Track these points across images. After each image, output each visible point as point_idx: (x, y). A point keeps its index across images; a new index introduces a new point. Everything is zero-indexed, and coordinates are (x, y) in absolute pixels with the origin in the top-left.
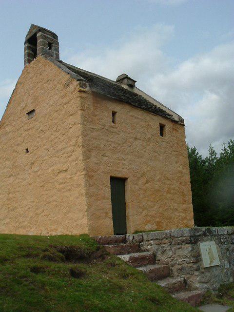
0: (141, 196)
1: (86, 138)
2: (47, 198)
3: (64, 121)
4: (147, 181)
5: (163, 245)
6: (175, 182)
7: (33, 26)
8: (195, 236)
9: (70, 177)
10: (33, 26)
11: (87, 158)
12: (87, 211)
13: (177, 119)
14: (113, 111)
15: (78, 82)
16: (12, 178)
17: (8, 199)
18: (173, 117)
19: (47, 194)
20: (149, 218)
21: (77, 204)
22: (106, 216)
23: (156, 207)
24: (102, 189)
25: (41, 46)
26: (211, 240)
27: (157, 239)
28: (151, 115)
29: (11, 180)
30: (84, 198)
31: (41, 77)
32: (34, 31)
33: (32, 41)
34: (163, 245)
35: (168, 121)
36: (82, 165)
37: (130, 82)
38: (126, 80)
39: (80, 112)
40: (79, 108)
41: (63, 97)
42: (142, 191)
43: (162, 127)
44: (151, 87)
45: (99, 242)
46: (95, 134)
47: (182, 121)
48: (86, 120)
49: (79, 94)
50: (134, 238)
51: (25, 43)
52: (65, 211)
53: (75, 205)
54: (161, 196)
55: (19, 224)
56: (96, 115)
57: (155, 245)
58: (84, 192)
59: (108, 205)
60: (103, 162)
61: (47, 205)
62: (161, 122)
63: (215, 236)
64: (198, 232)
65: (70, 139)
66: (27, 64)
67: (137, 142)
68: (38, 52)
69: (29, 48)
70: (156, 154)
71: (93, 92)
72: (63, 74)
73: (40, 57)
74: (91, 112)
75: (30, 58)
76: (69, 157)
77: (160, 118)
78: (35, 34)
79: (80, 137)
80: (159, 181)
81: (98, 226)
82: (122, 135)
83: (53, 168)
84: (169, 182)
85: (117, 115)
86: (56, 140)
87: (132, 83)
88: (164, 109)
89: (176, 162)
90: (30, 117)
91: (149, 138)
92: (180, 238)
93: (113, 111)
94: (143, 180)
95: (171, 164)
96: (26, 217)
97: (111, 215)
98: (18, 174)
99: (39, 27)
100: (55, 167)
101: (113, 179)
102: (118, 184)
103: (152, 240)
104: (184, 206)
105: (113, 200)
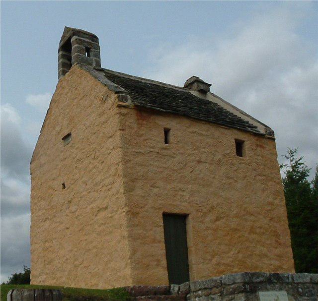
0: (210, 238)
1: (129, 165)
2: (86, 244)
3: (102, 145)
4: (217, 217)
5: (213, 296)
6: (261, 217)
7: (67, 29)
8: (253, 283)
9: (110, 215)
10: (67, 29)
11: (129, 189)
12: (130, 258)
13: (262, 131)
14: (165, 129)
15: (117, 95)
16: (48, 222)
17: (46, 249)
18: (258, 129)
19: (86, 240)
20: (222, 268)
21: (118, 249)
22: (158, 265)
23: (232, 253)
24: (151, 229)
25: (76, 54)
26: (281, 289)
27: (206, 289)
28: (222, 130)
29: (47, 223)
30: (127, 242)
31: (76, 91)
32: (68, 35)
33: (66, 47)
34: (213, 296)
35: (246, 134)
36: (123, 200)
37: (202, 87)
38: (196, 84)
39: (119, 133)
40: (118, 128)
41: (100, 115)
42: (210, 231)
43: (239, 145)
44: (222, 88)
45: (131, 294)
46: (140, 159)
47: (272, 133)
48: (127, 143)
49: (117, 110)
50: (179, 289)
51: (59, 51)
52: (106, 259)
53: (117, 251)
54: (240, 237)
55: (57, 280)
56: (142, 135)
57: (204, 297)
58: (126, 234)
59: (160, 250)
60: (152, 194)
61: (87, 253)
62: (237, 137)
63: (288, 284)
64: (258, 277)
65: (109, 168)
66: (62, 77)
67: (202, 166)
68: (73, 61)
69: (63, 56)
70: (231, 181)
71: (136, 106)
72: (100, 86)
73: (75, 67)
74: (133, 131)
75: (66, 69)
76: (109, 190)
77: (236, 132)
78: (70, 39)
79: (120, 164)
80: (237, 216)
81: (145, 278)
82: (179, 158)
83: (91, 206)
84: (252, 218)
85: (171, 133)
86: (94, 170)
87: (204, 88)
88: (245, 119)
89: (263, 191)
90: (67, 143)
91: (220, 160)
92: (233, 286)
93: (165, 129)
94: (211, 217)
95: (255, 193)
96: (64, 271)
97: (164, 262)
98: (55, 216)
99: (73, 30)
100: (94, 205)
101: (167, 216)
102: (175, 223)
103: (200, 290)
104: (277, 251)
105: (166, 242)
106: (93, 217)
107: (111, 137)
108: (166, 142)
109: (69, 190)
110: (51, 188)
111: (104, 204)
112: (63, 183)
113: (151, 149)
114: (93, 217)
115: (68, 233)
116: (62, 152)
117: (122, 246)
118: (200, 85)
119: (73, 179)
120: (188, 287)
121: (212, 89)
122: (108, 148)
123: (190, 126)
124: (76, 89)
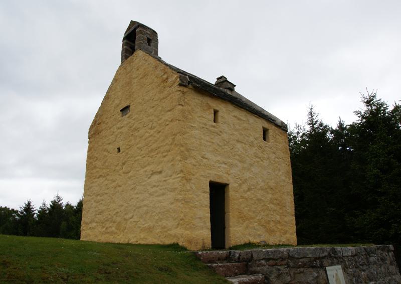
3: (161, 117)
7: (133, 23)
16: (101, 178)
37: (229, 86)
38: (225, 83)
61: (137, 210)
76: (164, 157)
85: (220, 114)
86: (150, 139)
98: (108, 175)
100: (148, 168)
102: (218, 192)
106: (146, 179)
107: (169, 111)
108: (215, 121)
109: (123, 154)
110: (106, 150)
111: (158, 169)
112: (118, 147)
113: (204, 126)
114: (146, 179)
115: (120, 191)
116: (120, 121)
117: (175, 208)
118: (228, 84)
119: (128, 145)
120: (250, 255)
121: (236, 89)
122: (167, 120)
123: (233, 111)
124: (138, 70)
